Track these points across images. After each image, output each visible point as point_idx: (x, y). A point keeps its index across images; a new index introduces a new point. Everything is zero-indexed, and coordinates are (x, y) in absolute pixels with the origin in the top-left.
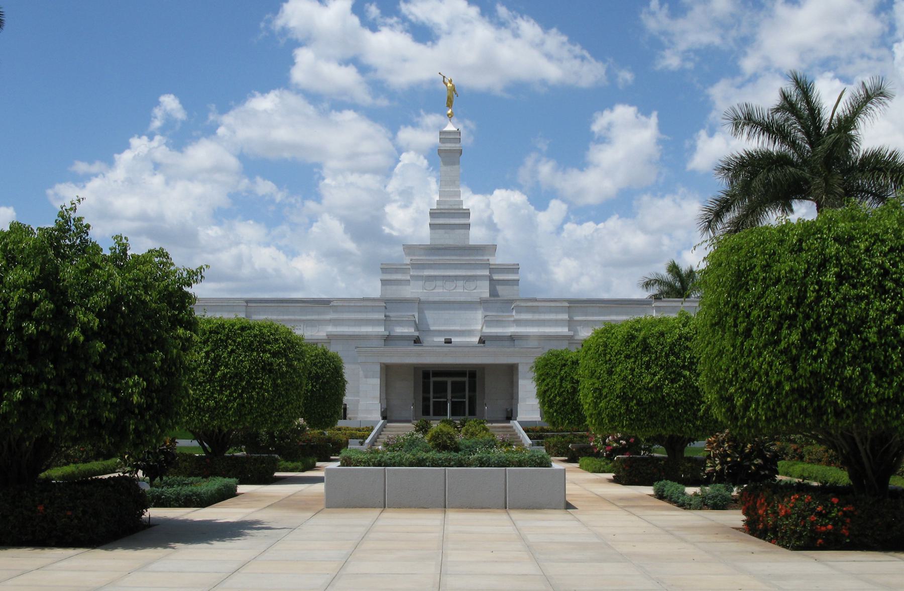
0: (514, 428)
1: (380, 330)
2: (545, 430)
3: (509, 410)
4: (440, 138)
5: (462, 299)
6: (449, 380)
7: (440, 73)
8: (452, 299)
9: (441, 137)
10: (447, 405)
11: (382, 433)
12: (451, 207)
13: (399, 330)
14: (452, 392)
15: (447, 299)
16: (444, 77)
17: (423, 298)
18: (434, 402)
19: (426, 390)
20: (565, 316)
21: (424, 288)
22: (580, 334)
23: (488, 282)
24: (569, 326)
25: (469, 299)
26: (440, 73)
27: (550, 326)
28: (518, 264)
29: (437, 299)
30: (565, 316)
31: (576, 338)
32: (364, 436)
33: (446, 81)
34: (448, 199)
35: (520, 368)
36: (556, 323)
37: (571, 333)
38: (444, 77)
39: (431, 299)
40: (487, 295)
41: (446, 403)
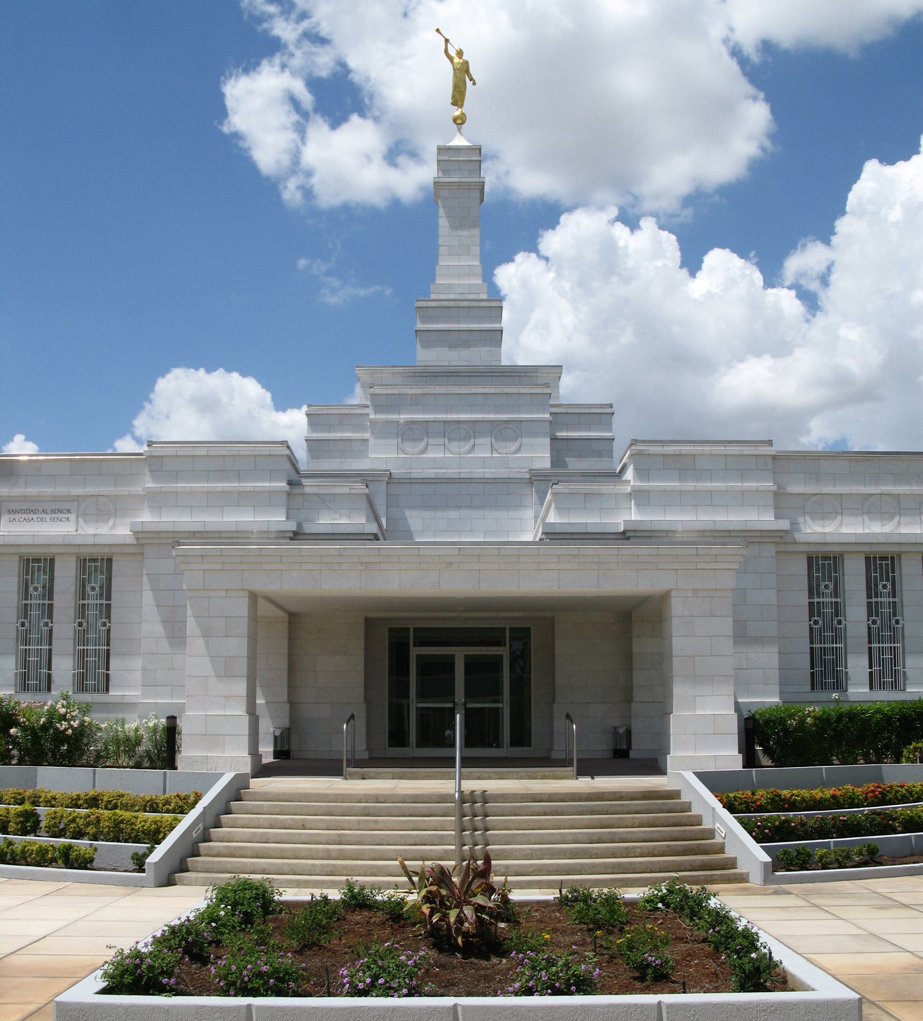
0: (684, 798)
1: (277, 518)
2: (784, 800)
3: (622, 731)
4: (439, 161)
5: (489, 473)
6: (460, 654)
7: (438, 30)
8: (465, 473)
9: (440, 158)
10: (454, 719)
11: (224, 818)
12: (461, 297)
13: (326, 521)
14: (466, 673)
15: (452, 472)
16: (447, 41)
17: (397, 471)
18: (422, 713)
19: (398, 690)
20: (769, 485)
21: (399, 449)
22: (802, 526)
23: (547, 441)
24: (777, 508)
25: (504, 473)
26: (438, 30)
27: (428, 792)
28: (611, 406)
29: (430, 473)
30: (769, 485)
31: (799, 537)
32: (157, 831)
33: (452, 52)
34: (456, 282)
35: (677, 607)
36: (743, 499)
37: (784, 525)
38: (447, 41)
39: (417, 473)
40: (547, 464)
41: (452, 713)
